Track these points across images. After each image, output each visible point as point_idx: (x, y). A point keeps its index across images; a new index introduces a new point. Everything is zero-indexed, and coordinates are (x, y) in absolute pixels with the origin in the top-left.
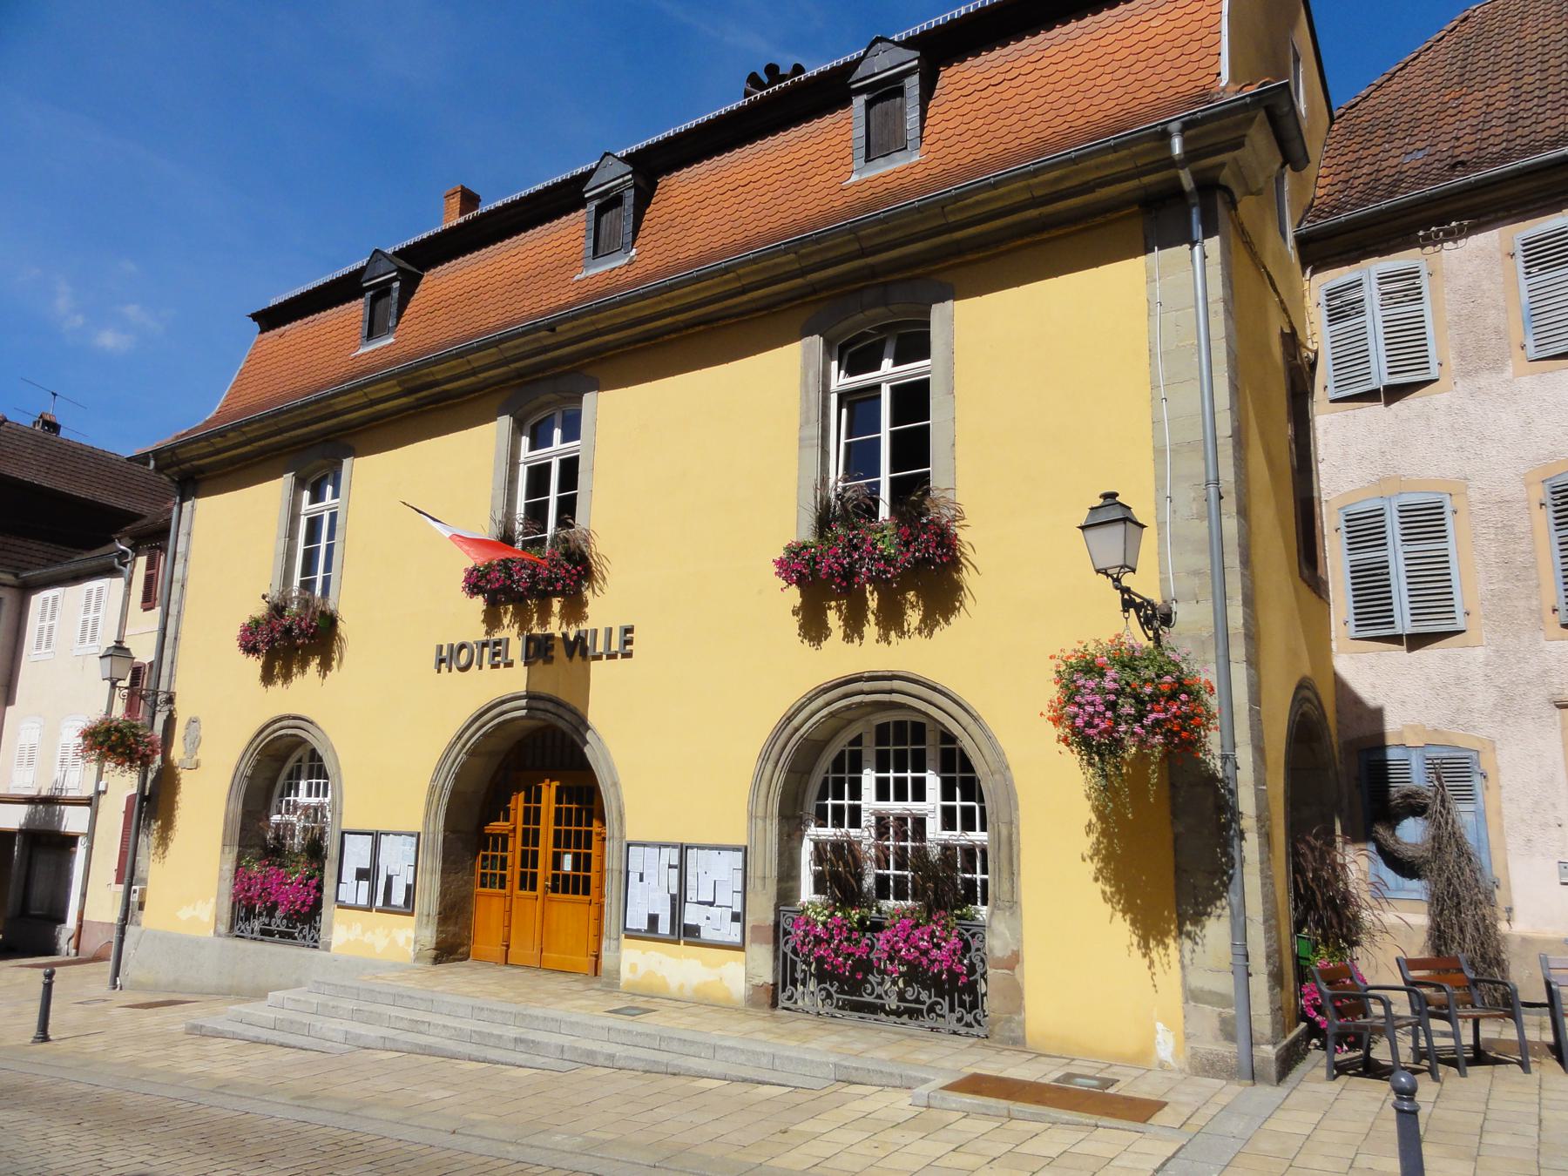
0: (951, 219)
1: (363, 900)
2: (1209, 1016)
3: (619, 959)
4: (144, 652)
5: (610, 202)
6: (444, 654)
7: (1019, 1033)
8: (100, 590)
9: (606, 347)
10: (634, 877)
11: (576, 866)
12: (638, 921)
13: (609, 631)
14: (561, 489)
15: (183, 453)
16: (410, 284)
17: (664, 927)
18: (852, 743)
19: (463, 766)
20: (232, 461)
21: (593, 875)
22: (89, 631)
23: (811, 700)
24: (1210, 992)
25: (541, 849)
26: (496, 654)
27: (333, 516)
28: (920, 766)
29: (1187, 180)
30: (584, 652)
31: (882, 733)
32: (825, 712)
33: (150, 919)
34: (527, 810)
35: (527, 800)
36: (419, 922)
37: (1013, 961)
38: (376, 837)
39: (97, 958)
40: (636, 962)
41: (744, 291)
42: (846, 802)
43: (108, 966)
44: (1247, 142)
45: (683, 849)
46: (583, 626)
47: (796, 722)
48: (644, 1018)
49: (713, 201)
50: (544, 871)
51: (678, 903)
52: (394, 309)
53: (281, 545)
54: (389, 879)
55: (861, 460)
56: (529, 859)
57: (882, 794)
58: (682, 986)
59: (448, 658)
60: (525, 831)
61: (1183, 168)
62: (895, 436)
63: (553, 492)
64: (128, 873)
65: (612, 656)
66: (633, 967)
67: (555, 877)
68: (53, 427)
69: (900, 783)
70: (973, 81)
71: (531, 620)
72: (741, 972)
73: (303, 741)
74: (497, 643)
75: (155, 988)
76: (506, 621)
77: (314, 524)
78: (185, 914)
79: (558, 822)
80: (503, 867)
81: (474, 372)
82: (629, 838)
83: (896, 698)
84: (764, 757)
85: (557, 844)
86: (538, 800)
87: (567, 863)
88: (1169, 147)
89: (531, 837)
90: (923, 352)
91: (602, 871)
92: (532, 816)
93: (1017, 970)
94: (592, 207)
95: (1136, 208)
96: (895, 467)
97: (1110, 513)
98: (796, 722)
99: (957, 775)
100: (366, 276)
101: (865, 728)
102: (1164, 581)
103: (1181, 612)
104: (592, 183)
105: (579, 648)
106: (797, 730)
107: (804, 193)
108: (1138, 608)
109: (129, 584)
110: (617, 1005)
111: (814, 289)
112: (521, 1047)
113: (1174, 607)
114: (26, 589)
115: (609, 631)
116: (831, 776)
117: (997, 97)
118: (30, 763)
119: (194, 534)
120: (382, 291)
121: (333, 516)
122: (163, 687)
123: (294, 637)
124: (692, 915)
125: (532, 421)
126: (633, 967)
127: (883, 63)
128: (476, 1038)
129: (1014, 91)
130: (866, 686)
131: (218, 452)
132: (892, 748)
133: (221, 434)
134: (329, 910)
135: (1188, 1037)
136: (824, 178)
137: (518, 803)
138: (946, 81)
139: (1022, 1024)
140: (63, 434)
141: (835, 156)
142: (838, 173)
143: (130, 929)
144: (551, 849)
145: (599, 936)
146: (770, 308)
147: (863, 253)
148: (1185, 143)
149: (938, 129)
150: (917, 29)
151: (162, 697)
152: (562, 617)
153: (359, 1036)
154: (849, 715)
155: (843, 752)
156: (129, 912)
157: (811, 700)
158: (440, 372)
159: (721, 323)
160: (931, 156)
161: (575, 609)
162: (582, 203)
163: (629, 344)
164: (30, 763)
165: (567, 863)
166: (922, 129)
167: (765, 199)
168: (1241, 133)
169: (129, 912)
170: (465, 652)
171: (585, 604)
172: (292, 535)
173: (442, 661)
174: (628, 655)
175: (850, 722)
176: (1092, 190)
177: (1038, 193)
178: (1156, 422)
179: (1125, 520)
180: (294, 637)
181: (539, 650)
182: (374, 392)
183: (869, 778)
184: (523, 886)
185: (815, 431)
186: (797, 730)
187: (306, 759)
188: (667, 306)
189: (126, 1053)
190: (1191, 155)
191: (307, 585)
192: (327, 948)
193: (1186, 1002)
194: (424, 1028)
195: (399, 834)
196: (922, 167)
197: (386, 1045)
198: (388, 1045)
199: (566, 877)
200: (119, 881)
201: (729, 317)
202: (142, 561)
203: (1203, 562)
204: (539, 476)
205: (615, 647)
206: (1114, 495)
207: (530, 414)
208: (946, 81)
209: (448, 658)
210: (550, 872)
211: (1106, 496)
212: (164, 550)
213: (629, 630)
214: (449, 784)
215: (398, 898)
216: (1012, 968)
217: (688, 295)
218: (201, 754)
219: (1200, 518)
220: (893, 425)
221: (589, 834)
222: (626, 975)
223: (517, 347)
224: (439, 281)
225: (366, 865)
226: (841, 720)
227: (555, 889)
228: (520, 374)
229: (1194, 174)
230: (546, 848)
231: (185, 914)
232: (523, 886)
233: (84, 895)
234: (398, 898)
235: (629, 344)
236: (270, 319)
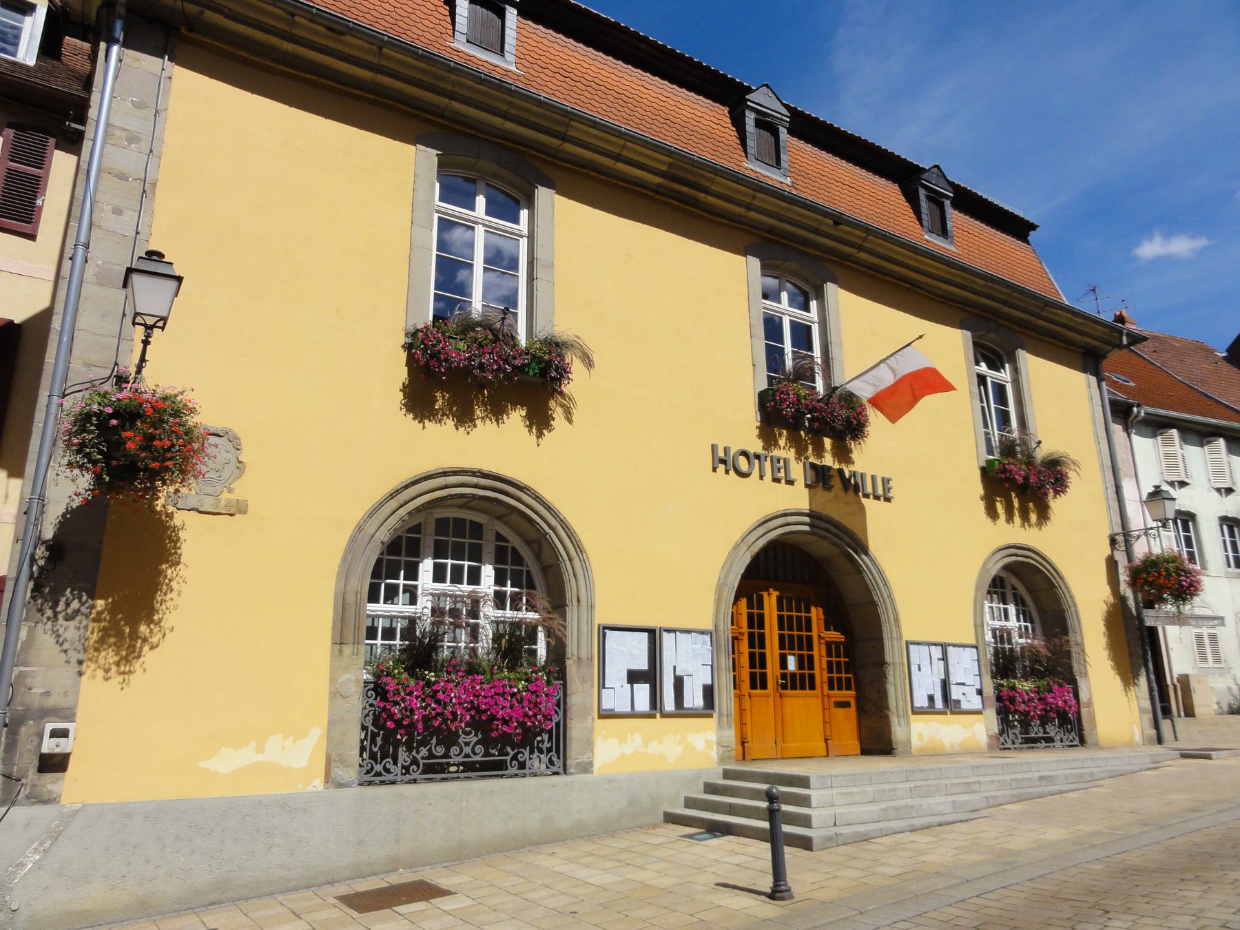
1: (643, 704)
9: (848, 257)
10: (914, 668)
11: (800, 665)
12: (921, 701)
17: (939, 704)
28: (476, 555)
30: (856, 488)
35: (750, 606)
42: (401, 582)
45: (944, 647)
46: (852, 468)
50: (772, 670)
51: (945, 685)
54: (679, 683)
57: (439, 576)
58: (952, 746)
67: (783, 676)
69: (457, 570)
71: (806, 449)
72: (980, 728)
76: (782, 442)
79: (781, 627)
80: (830, 664)
85: (782, 647)
86: (761, 606)
99: (509, 567)
105: (852, 486)
112: (1044, 783)
124: (955, 693)
126: (920, 735)
128: (1015, 785)
139: (1096, 735)
144: (777, 651)
152: (834, 455)
153: (967, 802)
155: (507, 541)
159: (919, 291)
161: (843, 454)
163: (865, 266)
171: (850, 451)
181: (820, 478)
184: (753, 686)
188: (912, 263)
192: (587, 768)
194: (975, 787)
195: (688, 632)
198: (991, 802)
199: (793, 675)
210: (778, 672)
215: (694, 698)
222: (915, 742)
223: (801, 215)
225: (642, 664)
227: (784, 687)
230: (772, 650)
232: (753, 686)
234: (694, 698)
235: (865, 266)
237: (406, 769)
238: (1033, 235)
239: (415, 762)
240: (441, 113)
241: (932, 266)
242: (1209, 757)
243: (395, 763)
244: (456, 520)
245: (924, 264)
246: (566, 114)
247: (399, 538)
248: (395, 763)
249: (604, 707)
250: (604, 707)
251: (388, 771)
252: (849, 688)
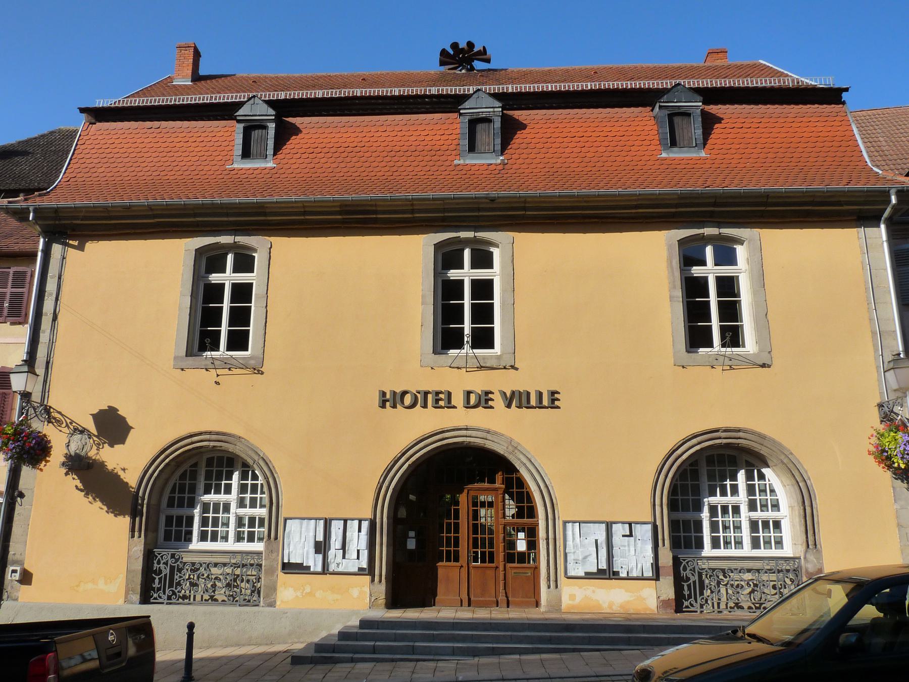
6: (388, 396)
18: (191, 466)
38: (345, 521)
54: (140, 537)
58: (610, 606)
66: (572, 597)
100: (665, 98)
104: (467, 104)
116: (679, 483)
126: (572, 597)
127: (258, 110)
130: (724, 435)
150: (282, 96)
155: (186, 471)
192: (272, 604)
200: (586, 573)
213: (553, 393)
237: (169, 598)
238: (845, 96)
242: (586, 573)
243: (164, 593)
244: (719, 455)
247: (685, 470)
248: (164, 593)
249: (614, 526)
250: (614, 526)
251: (160, 597)
252: (262, 506)
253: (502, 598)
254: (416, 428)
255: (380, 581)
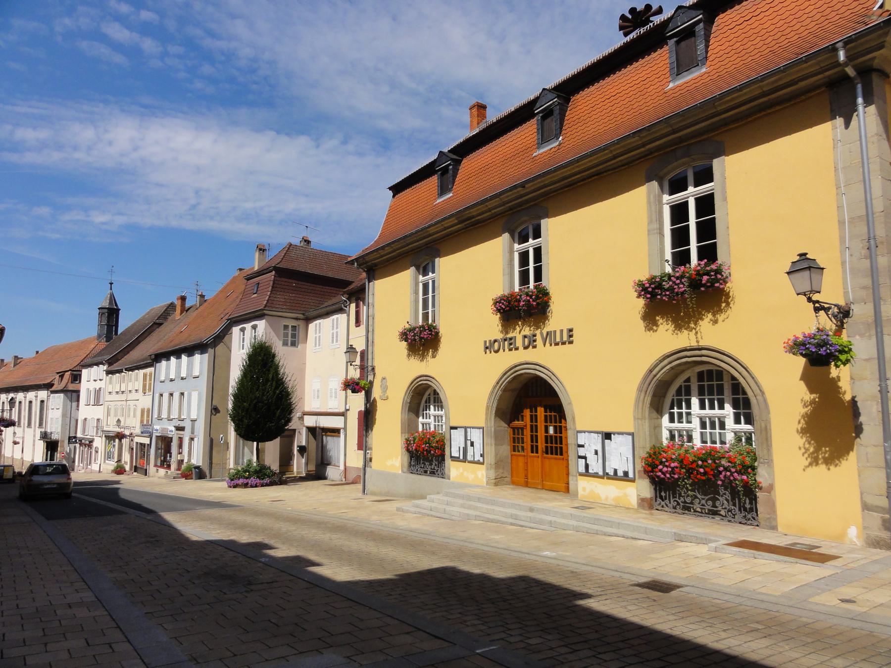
0: (719, 109)
2: (876, 519)
3: (577, 485)
4: (360, 346)
5: (548, 113)
7: (774, 523)
8: (337, 319)
11: (555, 431)
13: (562, 331)
14: (536, 281)
15: (367, 259)
16: (457, 163)
18: (685, 382)
19: (501, 397)
20: (388, 260)
21: (563, 446)
22: (335, 338)
23: (661, 361)
24: (877, 507)
25: (539, 434)
26: (511, 344)
27: (434, 282)
29: (850, 71)
31: (700, 376)
32: (668, 367)
33: (375, 465)
34: (531, 416)
36: (487, 469)
37: (771, 488)
39: (354, 482)
40: (584, 486)
41: (615, 157)
43: (360, 486)
44: (886, 44)
47: (654, 372)
48: (588, 511)
49: (599, 106)
52: (451, 179)
53: (413, 297)
55: (680, 237)
56: (534, 439)
58: (607, 498)
59: (489, 347)
60: (532, 426)
61: (847, 66)
62: (698, 224)
63: (532, 266)
64: (362, 445)
65: (564, 343)
66: (584, 489)
67: (546, 437)
68: (308, 242)
70: (734, 19)
73: (430, 386)
74: (511, 339)
75: (380, 494)
77: (426, 286)
78: (389, 463)
81: (490, 210)
82: (578, 429)
83: (704, 359)
84: (640, 390)
85: (546, 421)
87: (551, 430)
88: (837, 56)
89: (534, 429)
90: (710, 179)
91: (567, 445)
92: (534, 418)
93: (772, 493)
94: (539, 117)
95: (823, 89)
96: (699, 240)
97: (805, 266)
98: (654, 372)
100: (538, 105)
101: (692, 373)
102: (846, 293)
103: (856, 310)
106: (655, 376)
107: (645, 97)
108: (826, 310)
109: (348, 316)
110: (576, 505)
111: (651, 152)
113: (852, 307)
114: (308, 320)
115: (562, 331)
116: (675, 398)
117: (748, 28)
118: (318, 397)
119: (376, 294)
120: (445, 171)
121: (434, 282)
122: (370, 364)
123: (423, 340)
125: (519, 230)
126: (584, 489)
129: (758, 23)
131: (382, 256)
132: (706, 383)
133: (383, 248)
134: (448, 460)
135: (865, 528)
136: (655, 87)
137: (527, 413)
138: (720, 21)
140: (312, 246)
141: (661, 73)
142: (662, 83)
143: (368, 469)
145: (568, 474)
146: (629, 164)
147: (674, 132)
148: (847, 52)
149: (715, 51)
151: (370, 368)
154: (682, 368)
155: (681, 386)
156: (367, 461)
157: (661, 361)
158: (474, 212)
160: (712, 68)
162: (533, 116)
164: (318, 397)
165: (551, 430)
166: (707, 52)
167: (625, 102)
168: (882, 40)
169: (367, 461)
170: (496, 344)
172: (416, 292)
173: (487, 348)
174: (571, 342)
175: (683, 371)
176: (796, 83)
177: (765, 89)
178: (840, 207)
179: (809, 268)
180: (423, 340)
182: (446, 224)
183: (695, 401)
185: (656, 226)
186: (655, 376)
187: (432, 394)
188: (577, 169)
189: (375, 518)
190: (850, 58)
191: (426, 316)
193: (863, 511)
196: (707, 75)
197: (477, 518)
199: (551, 436)
201: (609, 170)
202: (353, 306)
203: (868, 282)
204: (524, 256)
205: (565, 338)
206: (805, 254)
207: (517, 228)
208: (720, 21)
209: (489, 347)
210: (544, 434)
211: (801, 255)
212: (363, 300)
213: (571, 330)
214: (495, 405)
216: (769, 492)
217: (586, 163)
218: (388, 393)
219: (866, 258)
220: (697, 217)
221: (561, 427)
222: (581, 492)
224: (470, 163)
226: (676, 372)
228: (511, 209)
229: (853, 67)
231: (389, 463)
233: (345, 455)
236: (397, 189)
239: (678, 504)
240: (413, 250)
241: (597, 158)
245: (585, 164)
246: (422, 230)
253: (522, 480)
254: (507, 360)
255: (134, 416)
